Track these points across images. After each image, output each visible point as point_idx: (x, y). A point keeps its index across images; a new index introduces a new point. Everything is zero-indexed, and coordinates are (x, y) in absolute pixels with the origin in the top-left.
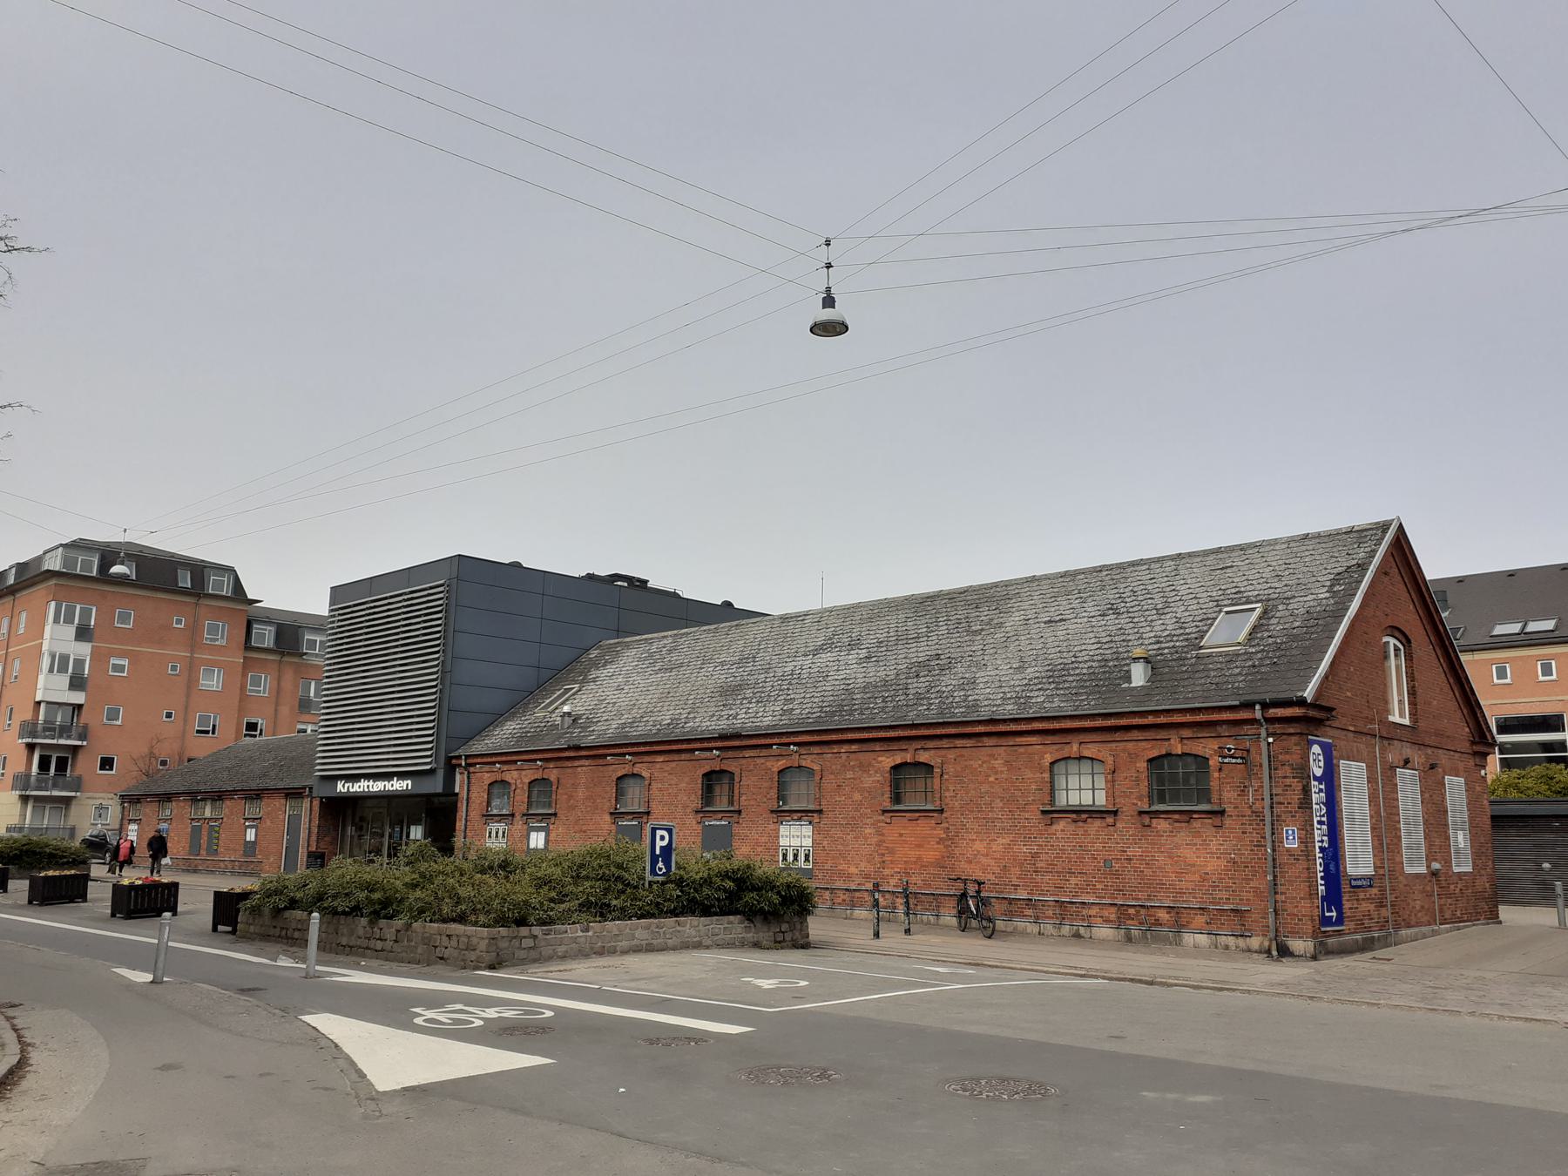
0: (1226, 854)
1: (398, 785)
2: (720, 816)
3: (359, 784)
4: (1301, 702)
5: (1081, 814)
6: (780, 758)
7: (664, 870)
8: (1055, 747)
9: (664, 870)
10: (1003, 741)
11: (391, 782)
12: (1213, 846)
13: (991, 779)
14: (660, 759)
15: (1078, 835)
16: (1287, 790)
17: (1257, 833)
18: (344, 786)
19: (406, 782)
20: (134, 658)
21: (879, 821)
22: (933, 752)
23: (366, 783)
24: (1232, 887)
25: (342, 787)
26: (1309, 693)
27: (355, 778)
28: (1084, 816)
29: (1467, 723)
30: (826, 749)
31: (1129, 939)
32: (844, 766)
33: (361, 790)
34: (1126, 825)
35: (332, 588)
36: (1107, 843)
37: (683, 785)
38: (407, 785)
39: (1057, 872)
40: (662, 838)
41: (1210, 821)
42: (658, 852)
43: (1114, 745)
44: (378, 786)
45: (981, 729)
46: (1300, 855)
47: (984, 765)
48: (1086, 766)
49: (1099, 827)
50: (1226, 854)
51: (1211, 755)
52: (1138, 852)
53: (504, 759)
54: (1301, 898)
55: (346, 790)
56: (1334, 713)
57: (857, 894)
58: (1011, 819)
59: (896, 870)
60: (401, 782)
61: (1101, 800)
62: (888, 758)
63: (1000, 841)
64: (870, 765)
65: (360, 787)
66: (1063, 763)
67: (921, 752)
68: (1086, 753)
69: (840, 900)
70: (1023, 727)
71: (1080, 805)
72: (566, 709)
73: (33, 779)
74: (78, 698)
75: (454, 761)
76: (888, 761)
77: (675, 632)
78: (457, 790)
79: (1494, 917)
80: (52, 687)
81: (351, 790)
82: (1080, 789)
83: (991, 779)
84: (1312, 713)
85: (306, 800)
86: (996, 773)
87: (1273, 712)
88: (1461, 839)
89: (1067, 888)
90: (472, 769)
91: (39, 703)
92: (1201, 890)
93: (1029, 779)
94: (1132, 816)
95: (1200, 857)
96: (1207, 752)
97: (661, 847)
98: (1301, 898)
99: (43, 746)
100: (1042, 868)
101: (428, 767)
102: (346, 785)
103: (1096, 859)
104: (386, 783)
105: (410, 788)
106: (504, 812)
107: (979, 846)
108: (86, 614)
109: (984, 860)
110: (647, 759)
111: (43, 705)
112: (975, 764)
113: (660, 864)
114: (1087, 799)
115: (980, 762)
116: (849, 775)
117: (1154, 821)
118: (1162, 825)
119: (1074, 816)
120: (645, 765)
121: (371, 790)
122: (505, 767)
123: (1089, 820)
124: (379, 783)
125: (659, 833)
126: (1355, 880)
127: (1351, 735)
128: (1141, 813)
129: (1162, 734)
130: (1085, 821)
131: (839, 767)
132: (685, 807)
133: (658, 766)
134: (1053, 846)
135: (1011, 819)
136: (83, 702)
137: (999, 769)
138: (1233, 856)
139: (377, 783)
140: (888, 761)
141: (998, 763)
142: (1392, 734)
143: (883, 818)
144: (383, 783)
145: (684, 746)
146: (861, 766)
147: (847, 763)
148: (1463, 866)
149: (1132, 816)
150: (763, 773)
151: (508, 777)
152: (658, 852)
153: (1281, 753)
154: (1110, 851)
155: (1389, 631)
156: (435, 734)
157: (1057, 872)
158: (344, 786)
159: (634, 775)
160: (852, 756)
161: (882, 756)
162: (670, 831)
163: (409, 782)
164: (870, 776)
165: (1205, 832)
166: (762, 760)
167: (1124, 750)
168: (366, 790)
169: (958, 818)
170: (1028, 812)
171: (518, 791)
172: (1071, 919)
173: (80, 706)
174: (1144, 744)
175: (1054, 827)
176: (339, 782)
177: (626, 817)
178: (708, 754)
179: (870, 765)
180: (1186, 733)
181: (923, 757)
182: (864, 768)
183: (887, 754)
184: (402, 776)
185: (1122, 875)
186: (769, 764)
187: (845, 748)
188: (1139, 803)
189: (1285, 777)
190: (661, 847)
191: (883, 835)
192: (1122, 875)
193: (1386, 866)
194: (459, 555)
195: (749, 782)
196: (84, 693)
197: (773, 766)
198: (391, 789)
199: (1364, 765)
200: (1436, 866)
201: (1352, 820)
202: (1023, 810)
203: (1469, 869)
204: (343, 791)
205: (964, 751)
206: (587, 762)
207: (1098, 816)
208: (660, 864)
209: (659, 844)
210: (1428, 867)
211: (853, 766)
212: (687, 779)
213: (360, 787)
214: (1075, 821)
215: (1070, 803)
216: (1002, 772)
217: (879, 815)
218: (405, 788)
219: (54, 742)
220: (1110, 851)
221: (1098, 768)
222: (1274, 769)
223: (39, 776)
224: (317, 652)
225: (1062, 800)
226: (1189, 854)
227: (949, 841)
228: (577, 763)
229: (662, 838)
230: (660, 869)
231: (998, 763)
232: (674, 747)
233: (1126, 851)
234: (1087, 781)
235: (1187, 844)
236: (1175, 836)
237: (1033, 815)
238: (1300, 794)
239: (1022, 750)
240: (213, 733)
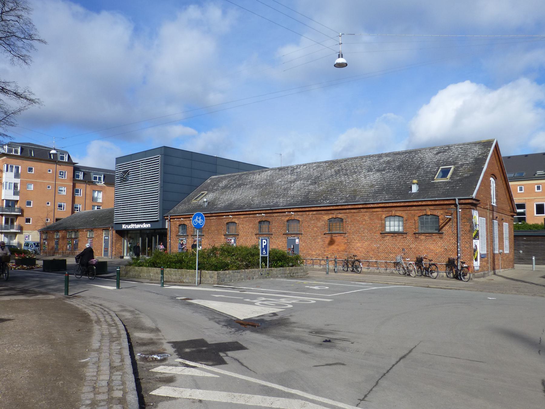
0: (444, 247)
1: (145, 226)
2: (265, 236)
3: (131, 225)
4: (472, 199)
5: (394, 234)
6: (287, 216)
7: (265, 253)
8: (386, 212)
9: (265, 253)
10: (368, 210)
11: (143, 225)
12: (439, 244)
13: (364, 223)
14: (242, 217)
15: (393, 241)
16: (465, 226)
17: (454, 240)
18: (125, 226)
19: (148, 225)
20: (35, 184)
21: (323, 237)
22: (343, 214)
23: (133, 225)
24: (445, 257)
25: (124, 227)
26: (474, 196)
27: (130, 223)
28: (396, 235)
29: (509, 206)
30: (304, 213)
31: (422, 274)
32: (311, 219)
33: (132, 227)
34: (410, 238)
35: (116, 158)
36: (403, 243)
37: (251, 226)
38: (128, 227)
39: (386, 253)
40: (265, 242)
41: (439, 236)
42: (263, 247)
43: (406, 212)
44: (138, 226)
45: (361, 206)
46: (469, 247)
47: (361, 219)
48: (397, 219)
49: (401, 238)
50: (444, 247)
51: (440, 215)
52: (414, 246)
53: (184, 216)
54: (468, 261)
55: (126, 228)
56: (480, 202)
57: (315, 261)
58: (370, 236)
59: (329, 253)
60: (146, 225)
61: (401, 229)
62: (327, 216)
63: (366, 243)
64: (320, 219)
65: (131, 227)
66: (389, 217)
67: (339, 214)
68: (397, 214)
69: (309, 263)
70: (376, 205)
71: (394, 231)
72: (205, 200)
73: (3, 226)
74: (17, 198)
75: (166, 218)
76: (326, 218)
77: (230, 174)
78: (167, 227)
79: (513, 267)
80: (8, 194)
81: (128, 228)
82: (395, 226)
83: (364, 223)
84: (474, 202)
85: (110, 231)
86: (365, 221)
87: (462, 201)
88: (506, 243)
89: (389, 258)
90: (172, 220)
91: (3, 200)
92: (435, 258)
93: (377, 223)
94: (412, 235)
95: (435, 248)
96: (439, 214)
97: (264, 245)
98: (468, 261)
99: (6, 215)
100: (381, 251)
101: (157, 220)
102: (126, 226)
103: (400, 248)
104: (141, 225)
105: (150, 227)
106: (185, 234)
107: (359, 245)
108: (17, 168)
109: (361, 249)
110: (237, 216)
111: (5, 201)
112: (358, 218)
113: (264, 251)
114: (396, 229)
115: (360, 218)
116: (313, 222)
117: (420, 237)
118: (422, 237)
119: (392, 235)
120: (237, 219)
121: (135, 227)
122: (185, 219)
123: (397, 236)
124: (138, 225)
125: (264, 241)
126: (482, 255)
127: (482, 209)
128: (414, 234)
129: (424, 208)
130: (396, 236)
131: (309, 219)
132: (252, 233)
133: (241, 219)
134: (385, 244)
135: (370, 236)
136: (18, 199)
137: (367, 220)
138: (446, 247)
139: (137, 225)
140: (326, 218)
141: (366, 218)
142: (492, 209)
143: (325, 236)
144: (140, 225)
145: (252, 212)
146: (317, 219)
147: (312, 218)
148: (507, 251)
149: (412, 235)
150: (281, 221)
151: (186, 223)
152: (263, 247)
153: (463, 215)
154: (404, 246)
155: (492, 176)
156: (158, 209)
157: (386, 253)
158: (125, 226)
159: (232, 222)
160: (314, 216)
161: (325, 216)
162: (267, 240)
163: (150, 225)
164: (320, 222)
165: (437, 240)
166: (280, 217)
167: (410, 213)
168: (134, 227)
169: (352, 236)
170: (376, 233)
171: (189, 227)
172: (390, 268)
173: (17, 201)
174: (417, 211)
175: (385, 238)
176: (123, 225)
177: (230, 236)
178: (260, 215)
179: (320, 219)
180: (432, 207)
181: (340, 216)
182: (318, 219)
183: (327, 215)
184: (147, 222)
185: (408, 253)
186: (283, 218)
187: (311, 213)
188: (415, 230)
189: (465, 222)
190: (264, 245)
191: (325, 242)
192: (408, 253)
193: (489, 251)
194: (164, 146)
195: (276, 225)
196: (19, 196)
197: (284, 219)
198: (143, 227)
199: (485, 219)
200: (501, 251)
201: (481, 236)
202: (375, 233)
203: (508, 252)
204: (125, 228)
205: (355, 214)
206: (215, 218)
207: (401, 234)
208: (264, 251)
209: (264, 244)
210: (499, 251)
211: (314, 219)
212: (252, 224)
213: (131, 227)
214: (392, 236)
215: (391, 231)
216: (367, 221)
217: (323, 235)
218: (148, 227)
219: (10, 213)
220: (404, 246)
221: (401, 219)
222: (461, 220)
223: (5, 225)
224: (98, 181)
225: (387, 229)
226: (432, 247)
227: (348, 243)
228: (211, 218)
229: (265, 242)
230: (264, 253)
231: (366, 218)
232: (248, 213)
233: (410, 246)
234: (396, 223)
235: (430, 244)
236: (427, 241)
237: (378, 235)
238: (469, 228)
239: (375, 213)
240: (64, 209)
